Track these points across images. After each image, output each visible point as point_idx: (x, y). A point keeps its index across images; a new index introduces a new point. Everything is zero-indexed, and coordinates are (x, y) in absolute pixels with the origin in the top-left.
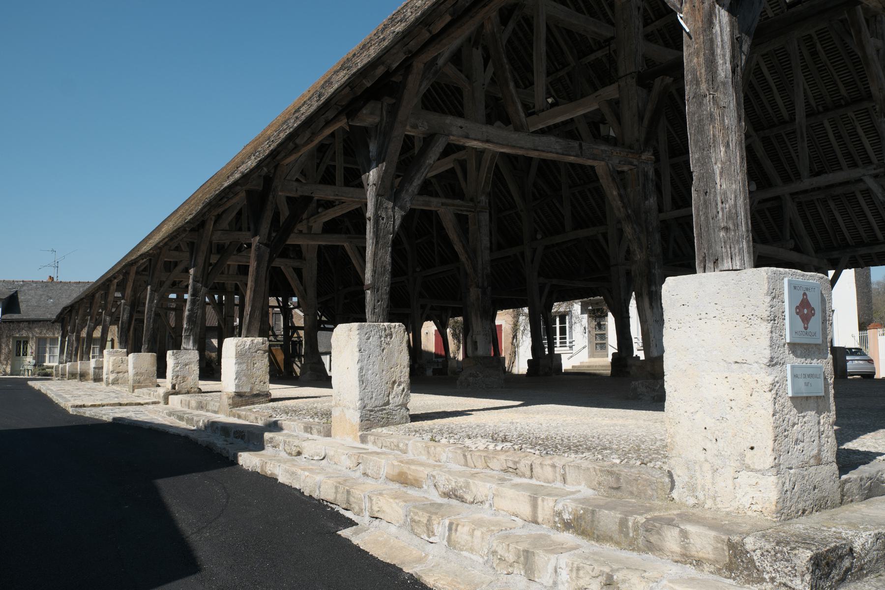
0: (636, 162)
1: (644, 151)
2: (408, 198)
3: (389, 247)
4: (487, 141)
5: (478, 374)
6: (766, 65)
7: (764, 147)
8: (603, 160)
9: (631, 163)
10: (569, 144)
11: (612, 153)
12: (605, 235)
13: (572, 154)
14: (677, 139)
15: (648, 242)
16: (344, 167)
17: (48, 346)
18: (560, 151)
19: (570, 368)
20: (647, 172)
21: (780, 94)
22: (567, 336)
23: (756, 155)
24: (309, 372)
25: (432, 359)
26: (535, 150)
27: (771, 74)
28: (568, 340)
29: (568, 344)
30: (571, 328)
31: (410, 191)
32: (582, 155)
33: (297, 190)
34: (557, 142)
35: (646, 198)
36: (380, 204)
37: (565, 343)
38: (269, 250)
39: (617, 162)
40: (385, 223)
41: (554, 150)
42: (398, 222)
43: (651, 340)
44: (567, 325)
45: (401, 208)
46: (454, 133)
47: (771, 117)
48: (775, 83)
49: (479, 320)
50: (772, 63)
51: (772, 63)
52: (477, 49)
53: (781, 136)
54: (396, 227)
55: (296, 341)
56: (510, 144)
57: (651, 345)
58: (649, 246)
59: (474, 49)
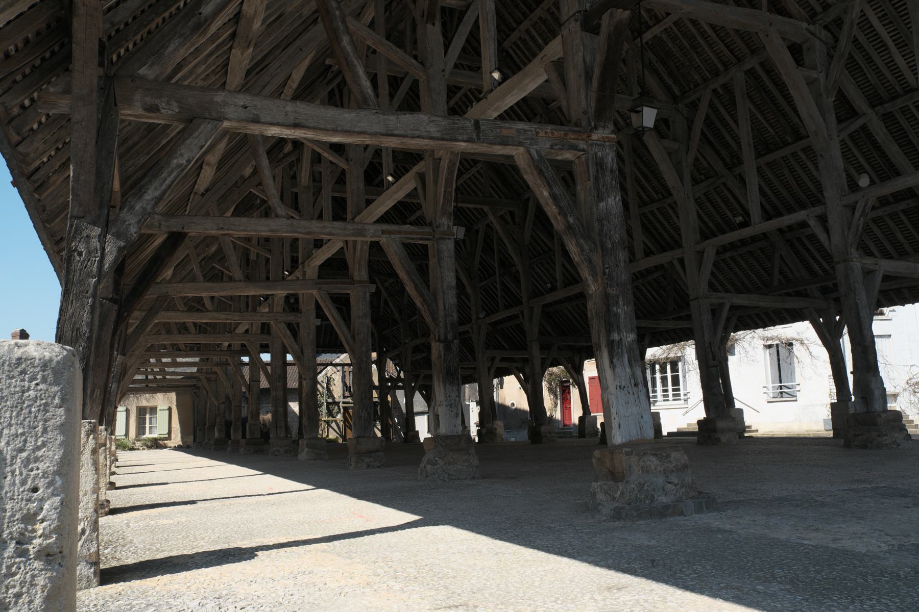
0: (582, 145)
1: (596, 128)
2: (132, 220)
3: (88, 298)
4: (296, 126)
5: (436, 461)
6: (876, 14)
7: (886, 127)
8: (520, 144)
9: (573, 147)
10: (454, 123)
11: (537, 133)
12: (681, 261)
13: (460, 138)
14: (770, 129)
15: (603, 265)
16: (333, 197)
17: (148, 416)
18: (438, 135)
19: (686, 426)
20: (602, 159)
21: (900, 52)
22: (681, 387)
23: (876, 140)
24: (306, 450)
25: (527, 419)
26: (387, 135)
27: (884, 25)
28: (682, 392)
29: (682, 397)
30: (684, 377)
31: (137, 208)
32: (479, 138)
33: (160, 225)
34: (432, 121)
35: (600, 198)
36: (75, 232)
37: (679, 395)
38: (116, 307)
39: (548, 145)
40: (84, 261)
41: (424, 134)
42: (109, 259)
43: (612, 418)
44: (680, 374)
45: (118, 236)
46: (231, 116)
47: (891, 85)
48: (891, 37)
49: (441, 385)
50: (883, 10)
51: (883, 10)
52: (434, 25)
53: (909, 109)
54: (106, 266)
55: (377, 402)
56: (339, 129)
57: (613, 426)
58: (607, 271)
59: (429, 26)
